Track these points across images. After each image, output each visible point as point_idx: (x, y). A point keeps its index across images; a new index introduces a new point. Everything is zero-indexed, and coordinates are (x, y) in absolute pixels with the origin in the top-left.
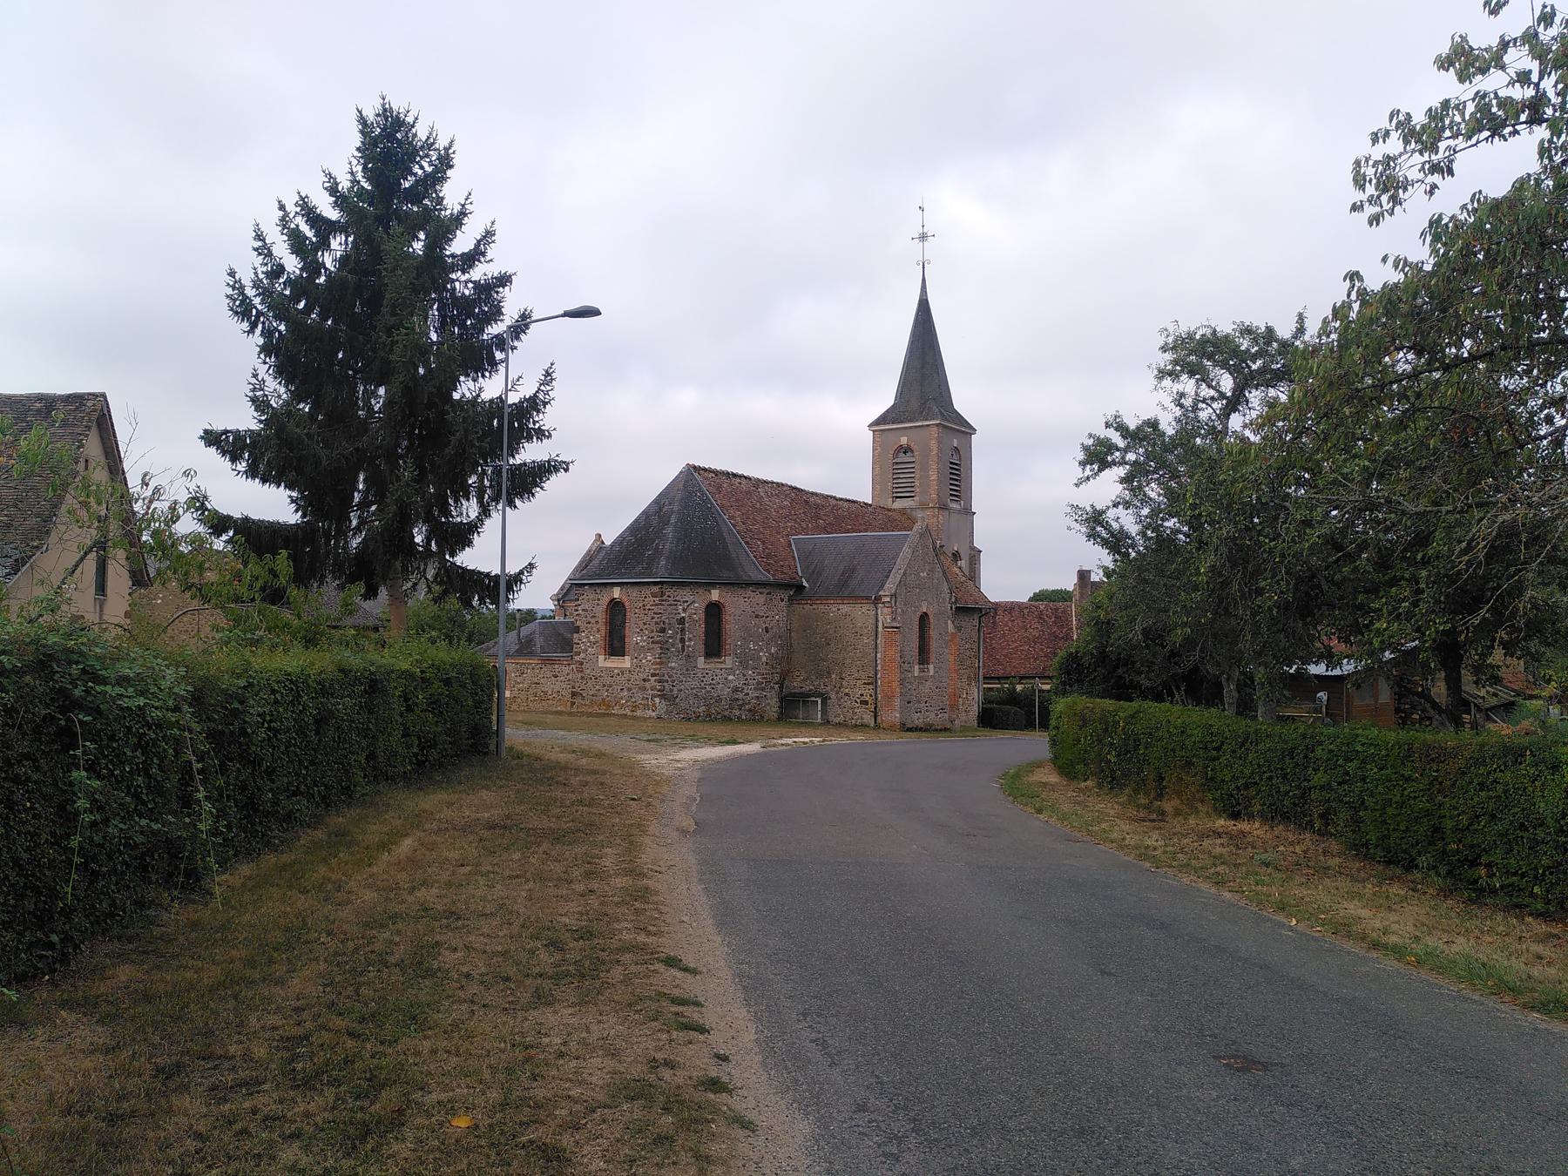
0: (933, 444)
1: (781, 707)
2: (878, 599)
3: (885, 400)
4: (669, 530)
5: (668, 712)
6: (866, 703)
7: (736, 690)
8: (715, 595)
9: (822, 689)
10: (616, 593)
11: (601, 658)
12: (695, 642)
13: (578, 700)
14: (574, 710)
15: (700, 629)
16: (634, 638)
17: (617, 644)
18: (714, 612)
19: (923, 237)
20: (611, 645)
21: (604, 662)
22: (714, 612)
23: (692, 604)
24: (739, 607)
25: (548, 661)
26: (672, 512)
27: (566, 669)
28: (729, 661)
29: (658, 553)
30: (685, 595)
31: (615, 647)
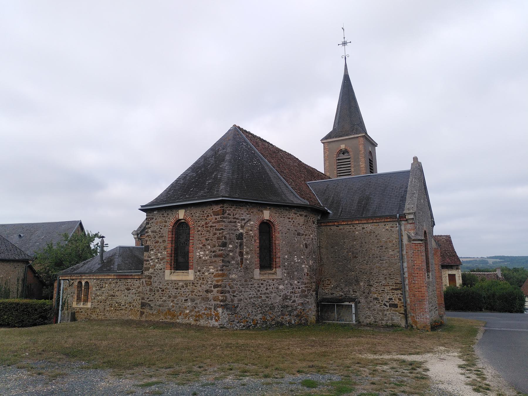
0: (361, 147)
1: (317, 311)
2: (403, 217)
3: (329, 128)
4: (226, 165)
5: (231, 321)
6: (395, 306)
7: (285, 298)
8: (266, 215)
9: (352, 295)
10: (181, 214)
11: (167, 272)
12: (252, 256)
13: (147, 310)
14: (143, 319)
15: (256, 244)
16: (198, 253)
17: (181, 259)
18: (266, 228)
19: (344, 44)
20: (176, 261)
21: (170, 276)
22: (266, 228)
23: (248, 222)
24: (288, 227)
25: (120, 277)
26: (226, 153)
27: (137, 283)
28: (279, 273)
29: (217, 181)
30: (242, 213)
31: (180, 261)
